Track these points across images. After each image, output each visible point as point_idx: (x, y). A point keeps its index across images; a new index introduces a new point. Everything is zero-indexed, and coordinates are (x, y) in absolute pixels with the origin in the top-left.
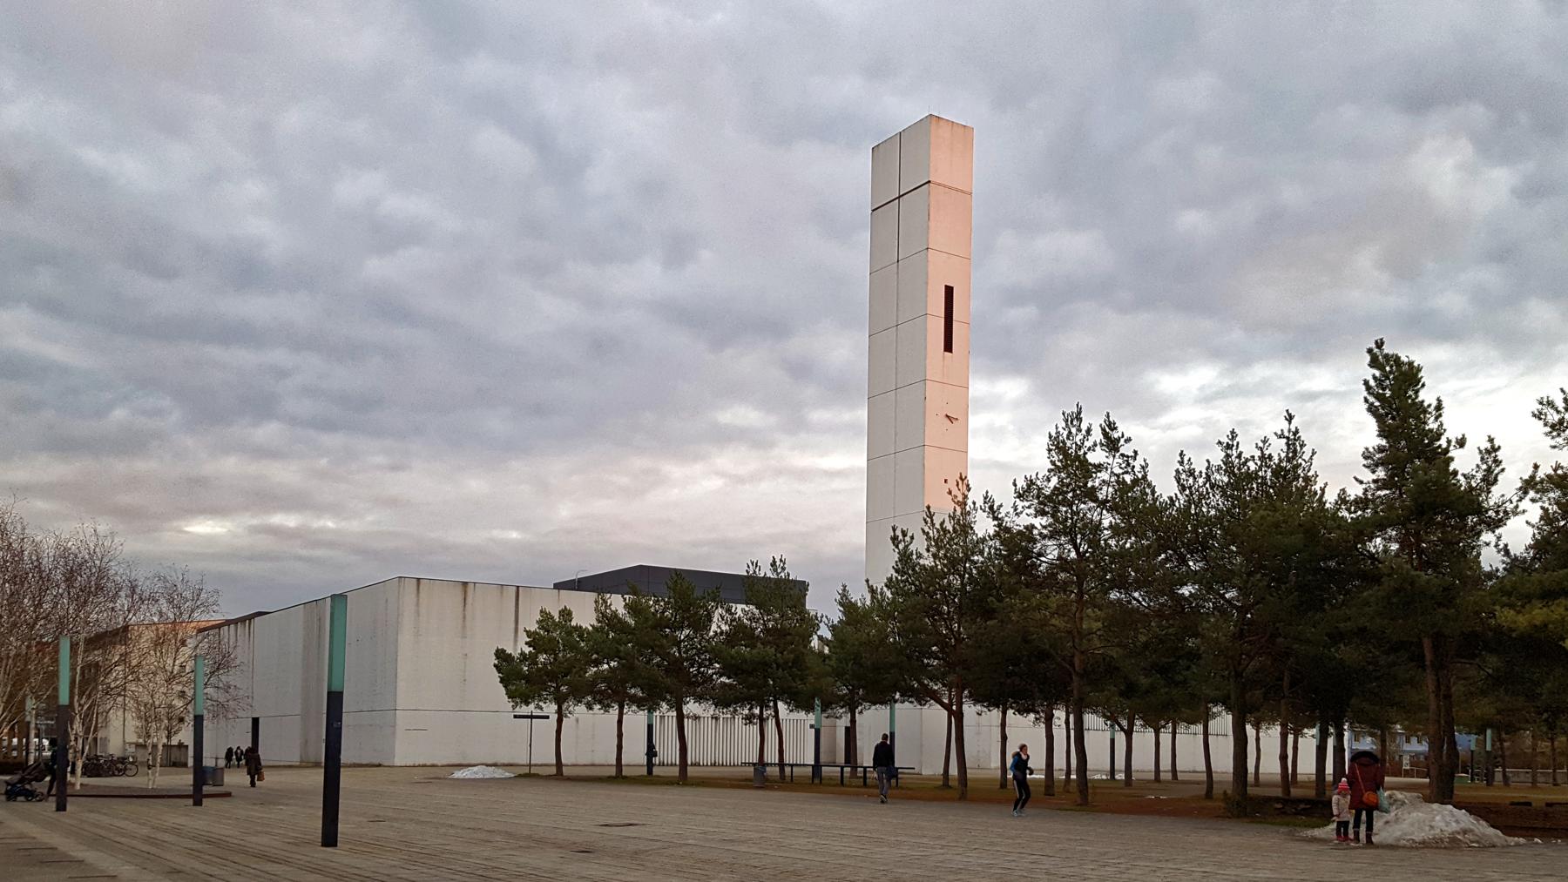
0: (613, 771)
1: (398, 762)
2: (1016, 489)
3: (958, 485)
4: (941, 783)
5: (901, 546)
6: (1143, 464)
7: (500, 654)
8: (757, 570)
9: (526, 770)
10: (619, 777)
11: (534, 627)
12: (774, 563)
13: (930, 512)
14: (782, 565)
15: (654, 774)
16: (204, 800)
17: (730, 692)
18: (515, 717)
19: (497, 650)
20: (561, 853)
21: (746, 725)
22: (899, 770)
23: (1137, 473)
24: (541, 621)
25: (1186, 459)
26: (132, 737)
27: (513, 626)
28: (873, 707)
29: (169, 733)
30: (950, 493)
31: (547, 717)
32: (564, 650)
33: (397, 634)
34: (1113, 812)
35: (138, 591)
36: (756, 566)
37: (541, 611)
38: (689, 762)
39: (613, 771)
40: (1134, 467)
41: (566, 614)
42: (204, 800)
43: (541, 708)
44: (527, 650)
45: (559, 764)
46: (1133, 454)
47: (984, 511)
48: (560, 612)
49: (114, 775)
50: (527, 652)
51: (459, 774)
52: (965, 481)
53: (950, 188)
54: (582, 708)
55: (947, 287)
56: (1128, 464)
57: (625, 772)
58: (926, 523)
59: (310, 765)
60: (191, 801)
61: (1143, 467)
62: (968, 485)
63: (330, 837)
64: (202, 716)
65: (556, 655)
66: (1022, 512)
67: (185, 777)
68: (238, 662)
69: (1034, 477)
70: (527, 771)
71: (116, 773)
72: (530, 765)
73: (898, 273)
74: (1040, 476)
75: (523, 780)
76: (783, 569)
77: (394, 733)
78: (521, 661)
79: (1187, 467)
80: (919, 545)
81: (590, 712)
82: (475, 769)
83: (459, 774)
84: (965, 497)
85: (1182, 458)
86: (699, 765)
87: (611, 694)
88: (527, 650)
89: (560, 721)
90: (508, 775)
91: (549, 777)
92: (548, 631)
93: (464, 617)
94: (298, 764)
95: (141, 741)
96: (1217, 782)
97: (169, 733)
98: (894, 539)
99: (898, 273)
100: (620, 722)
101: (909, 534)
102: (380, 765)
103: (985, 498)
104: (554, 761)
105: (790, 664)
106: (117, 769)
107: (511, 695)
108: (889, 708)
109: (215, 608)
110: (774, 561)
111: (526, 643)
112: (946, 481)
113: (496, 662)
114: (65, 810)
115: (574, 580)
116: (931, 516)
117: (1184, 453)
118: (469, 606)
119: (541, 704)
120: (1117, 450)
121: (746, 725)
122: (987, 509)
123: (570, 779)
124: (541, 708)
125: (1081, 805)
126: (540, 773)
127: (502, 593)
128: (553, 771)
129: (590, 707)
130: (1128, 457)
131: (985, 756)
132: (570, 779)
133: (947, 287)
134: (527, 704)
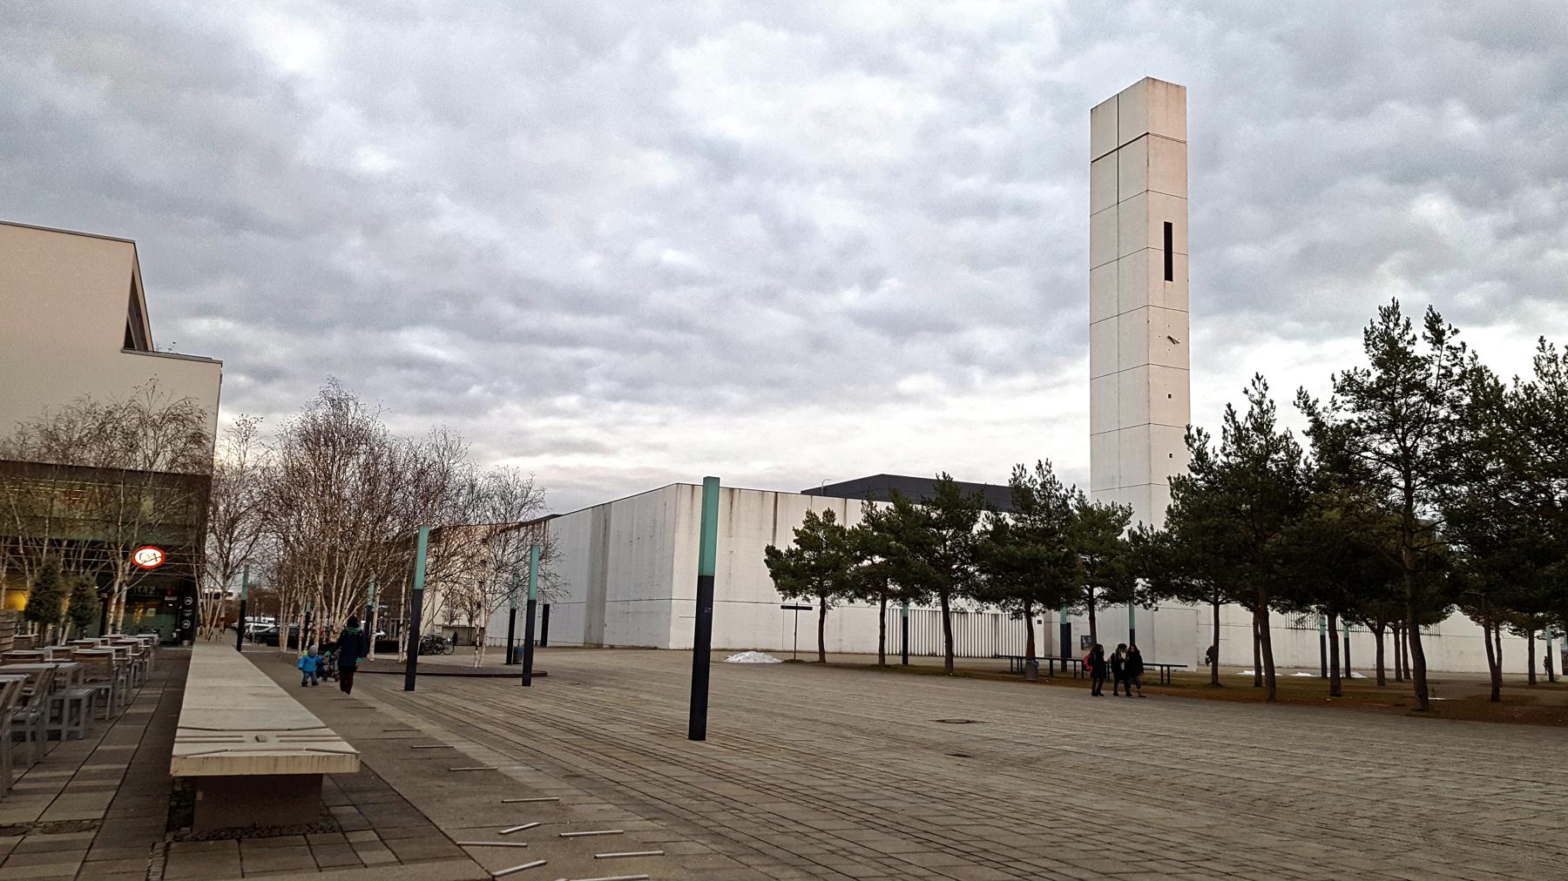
0: (876, 660)
1: (672, 646)
2: (1335, 384)
3: (1254, 384)
4: (1210, 681)
5: (1196, 445)
6: (1473, 356)
7: (771, 551)
8: (1023, 473)
9: (791, 656)
10: (881, 666)
11: (801, 527)
12: (1040, 466)
13: (1231, 410)
14: (1048, 468)
15: (909, 663)
16: (532, 679)
17: (1002, 588)
18: (783, 607)
19: (768, 547)
20: (958, 760)
21: (1012, 619)
22: (1144, 666)
23: (1466, 366)
24: (807, 521)
25: (1547, 345)
26: (439, 620)
27: (772, 527)
28: (1113, 605)
29: (471, 616)
30: (1246, 392)
31: (810, 609)
32: (827, 548)
33: (674, 532)
34: (1237, 701)
35: (476, 489)
36: (1023, 469)
37: (807, 513)
38: (909, 652)
39: (876, 660)
40: (1462, 359)
41: (829, 515)
42: (532, 679)
43: (808, 600)
44: (794, 547)
45: (822, 651)
46: (1461, 346)
47: (1299, 407)
48: (824, 513)
49: (433, 654)
50: (793, 549)
51: (733, 659)
52: (1262, 381)
53: (1167, 138)
54: (844, 601)
55: (1165, 223)
56: (1456, 357)
57: (828, 658)
58: (1227, 421)
59: (593, 646)
60: (520, 681)
61: (1472, 360)
62: (1265, 385)
63: (697, 730)
64: (535, 601)
65: (820, 552)
66: (1340, 407)
67: (501, 655)
68: (557, 553)
69: (1352, 372)
70: (793, 658)
71: (435, 651)
72: (795, 652)
73: (1118, 214)
74: (1358, 371)
75: (791, 666)
76: (1049, 472)
77: (669, 620)
78: (788, 557)
79: (1550, 352)
80: (1215, 445)
81: (851, 604)
82: (747, 654)
83: (733, 659)
84: (1263, 396)
85: (1543, 344)
86: (936, 656)
87: (868, 586)
88: (794, 547)
89: (823, 612)
90: (776, 660)
91: (813, 664)
92: (813, 531)
93: (731, 519)
94: (582, 645)
95: (447, 623)
96: (1433, 682)
97: (471, 616)
98: (1188, 437)
99: (1118, 214)
100: (882, 615)
101: (1204, 433)
102: (655, 648)
103: (1300, 394)
104: (877, 651)
105: (1061, 562)
106: (436, 648)
107: (780, 588)
108: (1128, 606)
109: (541, 505)
110: (1040, 465)
111: (795, 541)
112: (1170, 396)
113: (766, 557)
114: (413, 690)
115: (820, 488)
116: (1233, 414)
117: (1544, 338)
118: (735, 509)
119: (808, 596)
120: (1441, 342)
121: (1012, 619)
122: (1302, 405)
123: (837, 666)
124: (808, 600)
125: (1422, 710)
126: (804, 660)
127: (763, 499)
128: (817, 658)
129: (851, 601)
130: (1455, 349)
131: (1239, 653)
132: (837, 666)
133: (1165, 223)
134: (795, 596)
